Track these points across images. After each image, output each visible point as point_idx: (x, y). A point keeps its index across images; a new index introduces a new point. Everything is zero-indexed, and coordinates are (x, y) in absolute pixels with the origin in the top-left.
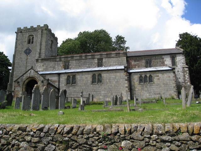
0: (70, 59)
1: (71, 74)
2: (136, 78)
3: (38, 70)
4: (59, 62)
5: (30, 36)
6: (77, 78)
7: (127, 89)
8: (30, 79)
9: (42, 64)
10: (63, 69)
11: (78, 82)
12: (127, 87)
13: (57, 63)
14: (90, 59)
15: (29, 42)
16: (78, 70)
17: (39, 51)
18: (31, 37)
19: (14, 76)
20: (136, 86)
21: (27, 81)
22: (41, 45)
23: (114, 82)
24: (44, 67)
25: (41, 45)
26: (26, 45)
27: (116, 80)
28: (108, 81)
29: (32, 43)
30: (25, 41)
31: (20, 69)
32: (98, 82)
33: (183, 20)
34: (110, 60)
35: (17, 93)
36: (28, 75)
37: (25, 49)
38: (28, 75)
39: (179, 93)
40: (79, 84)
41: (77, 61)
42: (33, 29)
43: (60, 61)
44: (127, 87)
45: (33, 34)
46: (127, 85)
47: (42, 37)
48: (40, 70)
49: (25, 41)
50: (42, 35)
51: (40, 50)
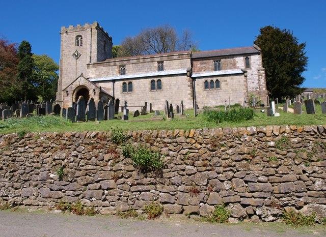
0: (125, 62)
5: (78, 36)
7: (190, 96)
9: (94, 70)
10: (119, 75)
13: (110, 67)
18: (80, 38)
23: (175, 89)
26: (73, 48)
37: (73, 52)
38: (77, 83)
40: (137, 92)
45: (81, 35)
49: (73, 44)
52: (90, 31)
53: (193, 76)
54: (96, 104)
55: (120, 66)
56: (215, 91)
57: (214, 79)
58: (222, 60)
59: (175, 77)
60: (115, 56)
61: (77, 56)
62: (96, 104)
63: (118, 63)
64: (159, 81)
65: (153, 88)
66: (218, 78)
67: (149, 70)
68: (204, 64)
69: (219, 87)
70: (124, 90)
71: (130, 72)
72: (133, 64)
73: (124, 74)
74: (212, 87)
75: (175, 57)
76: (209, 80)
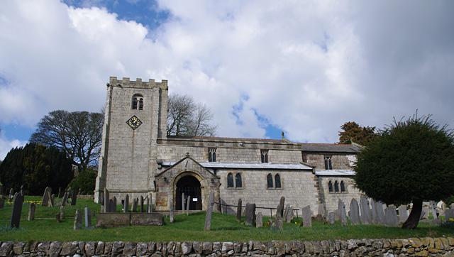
0: (217, 145)
1: (235, 171)
2: (325, 181)
3: (163, 158)
4: (199, 149)
5: (136, 95)
6: (244, 179)
7: (317, 199)
8: (185, 174)
9: (169, 149)
10: (207, 161)
11: (247, 185)
12: (317, 197)
13: (195, 149)
14: (249, 149)
15: (134, 107)
16: (232, 164)
17: (157, 124)
18: (138, 99)
19: (108, 165)
20: (325, 195)
21: (180, 177)
22: (159, 114)
23: (299, 189)
24: (174, 154)
25: (159, 114)
26: (129, 112)
27: (301, 186)
28: (290, 185)
29: (141, 108)
30: (128, 104)
31: (121, 152)
32: (276, 187)
33: (52, 114)
34: (280, 154)
35: (162, 197)
36: (183, 169)
37: (128, 117)
38: (182, 167)
39: (220, 210)
40: (248, 188)
41: (229, 150)
42: (145, 85)
43: (202, 146)
44: (317, 197)
45: (143, 94)
46: (317, 194)
47: (160, 100)
48: (167, 158)
49: (128, 104)
50: (160, 97)
51: (159, 123)
52: (158, 92)
53: (317, 173)
54: (358, 201)
55: (209, 148)
56: (341, 195)
57: (339, 180)
58: (334, 157)
59: (298, 173)
60: (270, 126)
61: (134, 124)
62: (358, 201)
63: (205, 144)
64: (277, 176)
65: (270, 185)
66: (344, 179)
67: (253, 159)
68: (315, 159)
69: (344, 191)
70: (230, 184)
71: (225, 158)
72: (227, 148)
73: (214, 160)
74: (337, 190)
75: (283, 147)
76: (333, 180)
